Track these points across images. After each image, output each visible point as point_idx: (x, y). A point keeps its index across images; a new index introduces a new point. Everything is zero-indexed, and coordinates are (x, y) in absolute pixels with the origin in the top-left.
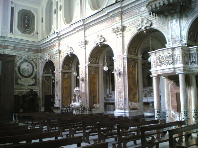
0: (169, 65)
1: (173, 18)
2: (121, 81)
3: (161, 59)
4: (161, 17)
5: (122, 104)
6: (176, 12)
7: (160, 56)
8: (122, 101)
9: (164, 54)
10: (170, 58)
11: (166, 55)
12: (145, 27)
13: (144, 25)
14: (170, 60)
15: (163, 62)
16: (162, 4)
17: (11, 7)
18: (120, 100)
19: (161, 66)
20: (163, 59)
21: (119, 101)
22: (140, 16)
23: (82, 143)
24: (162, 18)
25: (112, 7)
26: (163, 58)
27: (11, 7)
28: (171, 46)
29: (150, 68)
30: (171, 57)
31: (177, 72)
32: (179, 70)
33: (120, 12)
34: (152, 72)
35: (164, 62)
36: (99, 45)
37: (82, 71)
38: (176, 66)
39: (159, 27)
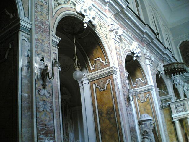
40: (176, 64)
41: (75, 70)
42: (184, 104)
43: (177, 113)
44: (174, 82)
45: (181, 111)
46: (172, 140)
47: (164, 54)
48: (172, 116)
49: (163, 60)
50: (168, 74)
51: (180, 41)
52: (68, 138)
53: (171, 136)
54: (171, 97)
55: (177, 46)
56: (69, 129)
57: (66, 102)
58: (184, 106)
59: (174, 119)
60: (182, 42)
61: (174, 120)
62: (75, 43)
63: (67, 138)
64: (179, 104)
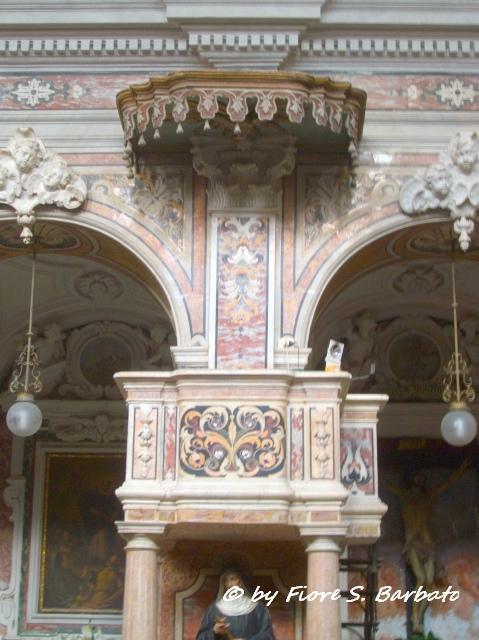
1: (240, 201)
3: (207, 427)
4: (154, 178)
6: (261, 180)
7: (201, 409)
9: (232, 406)
10: (269, 437)
11: (243, 411)
12: (39, 208)
13: (40, 188)
14: (268, 449)
15: (218, 454)
16: (266, 110)
19: (201, 474)
20: (225, 432)
22: (24, 128)
24: (160, 186)
26: (220, 425)
28: (212, 364)
29: (120, 479)
30: (274, 431)
31: (307, 525)
32: (316, 515)
33: (281, 60)
34: (128, 506)
35: (226, 453)
36: (21, 227)
38: (301, 488)
39: (140, 232)
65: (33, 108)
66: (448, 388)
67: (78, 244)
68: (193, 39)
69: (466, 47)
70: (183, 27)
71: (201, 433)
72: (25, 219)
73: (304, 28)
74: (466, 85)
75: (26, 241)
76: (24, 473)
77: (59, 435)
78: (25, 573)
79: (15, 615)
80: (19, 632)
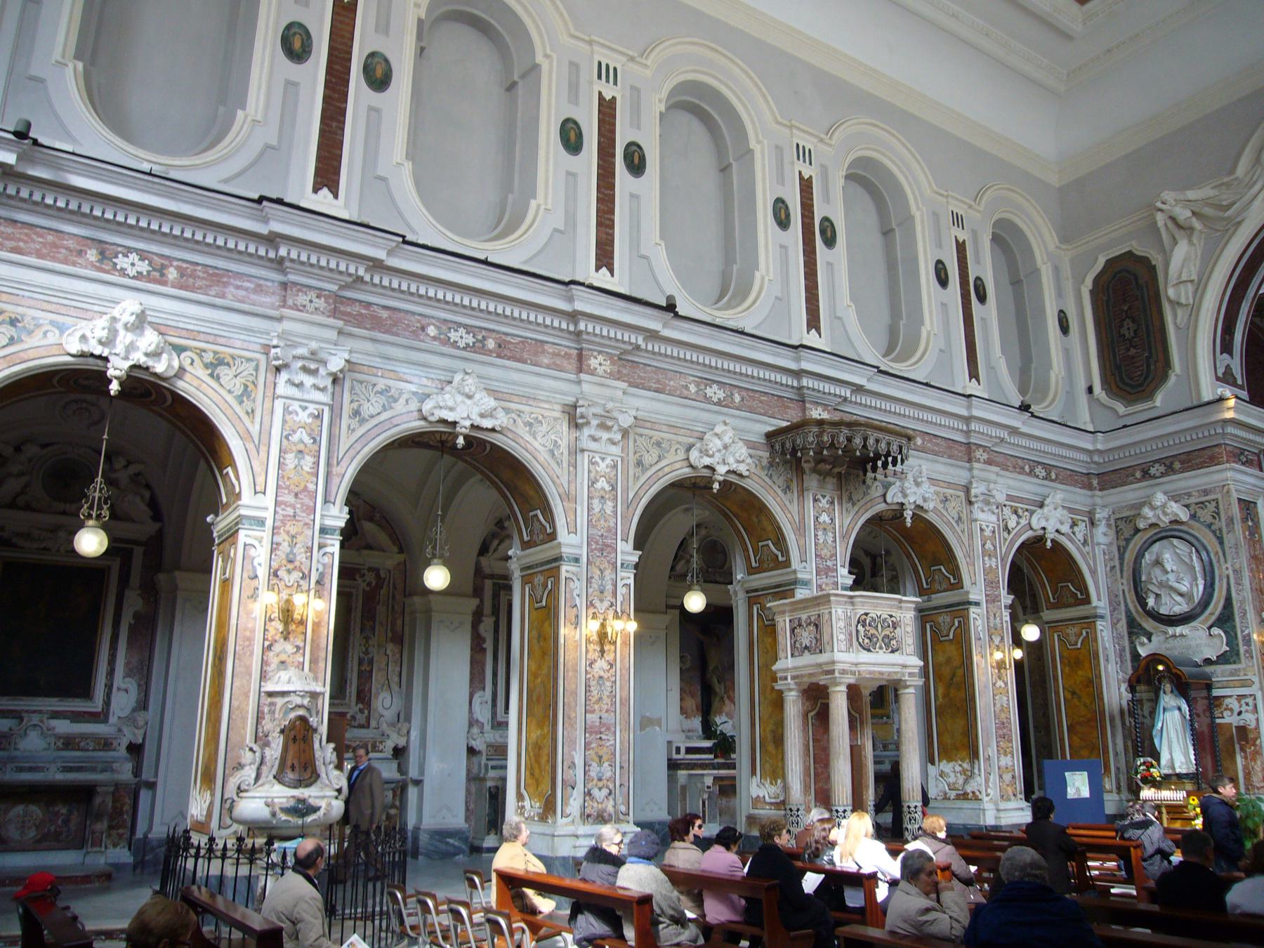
0: (893, 652)
2: (606, 675)
5: (605, 792)
7: (866, 614)
8: (609, 774)
11: (883, 617)
13: (731, 460)
17: (601, 97)
18: (594, 771)
21: (593, 774)
23: (1085, 773)
25: (715, 332)
27: (601, 97)
37: (285, 547)
40: (815, 429)
41: (81, 525)
42: (819, 615)
43: (792, 655)
44: (885, 501)
45: (806, 647)
46: (774, 771)
47: (798, 374)
48: (774, 668)
49: (804, 401)
50: (814, 470)
51: (1096, 259)
52: (366, 712)
53: (774, 752)
54: (793, 577)
55: (1083, 281)
56: (377, 678)
57: (378, 575)
58: (816, 626)
59: (781, 679)
60: (1109, 263)
61: (779, 682)
62: (105, 437)
63: (361, 711)
64: (804, 617)
65: (715, 404)
66: (85, 506)
67: (153, 397)
68: (283, 252)
69: (669, 350)
70: (278, 239)
71: (868, 628)
72: (463, 430)
73: (371, 264)
74: (468, 333)
75: (459, 446)
76: (493, 614)
77: (15, 540)
78: (495, 684)
79: (489, 715)
80: (493, 728)
